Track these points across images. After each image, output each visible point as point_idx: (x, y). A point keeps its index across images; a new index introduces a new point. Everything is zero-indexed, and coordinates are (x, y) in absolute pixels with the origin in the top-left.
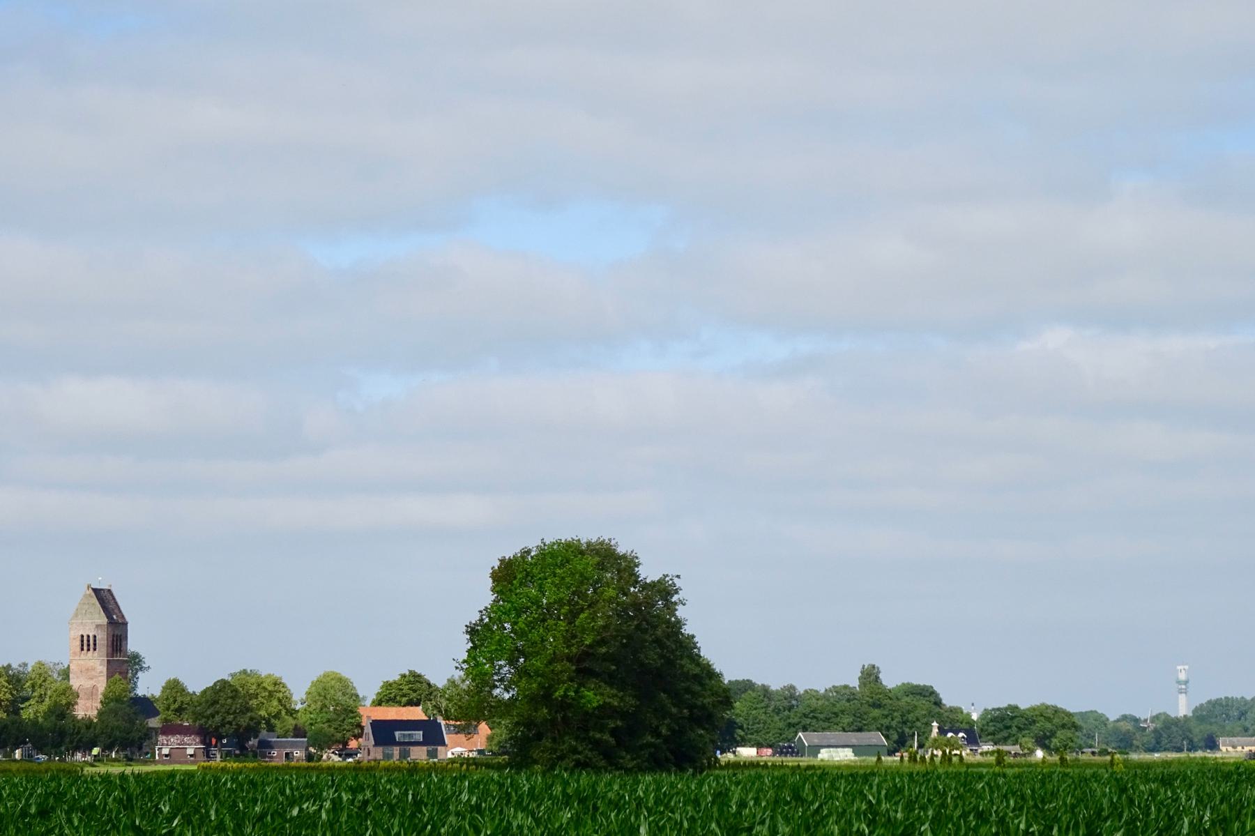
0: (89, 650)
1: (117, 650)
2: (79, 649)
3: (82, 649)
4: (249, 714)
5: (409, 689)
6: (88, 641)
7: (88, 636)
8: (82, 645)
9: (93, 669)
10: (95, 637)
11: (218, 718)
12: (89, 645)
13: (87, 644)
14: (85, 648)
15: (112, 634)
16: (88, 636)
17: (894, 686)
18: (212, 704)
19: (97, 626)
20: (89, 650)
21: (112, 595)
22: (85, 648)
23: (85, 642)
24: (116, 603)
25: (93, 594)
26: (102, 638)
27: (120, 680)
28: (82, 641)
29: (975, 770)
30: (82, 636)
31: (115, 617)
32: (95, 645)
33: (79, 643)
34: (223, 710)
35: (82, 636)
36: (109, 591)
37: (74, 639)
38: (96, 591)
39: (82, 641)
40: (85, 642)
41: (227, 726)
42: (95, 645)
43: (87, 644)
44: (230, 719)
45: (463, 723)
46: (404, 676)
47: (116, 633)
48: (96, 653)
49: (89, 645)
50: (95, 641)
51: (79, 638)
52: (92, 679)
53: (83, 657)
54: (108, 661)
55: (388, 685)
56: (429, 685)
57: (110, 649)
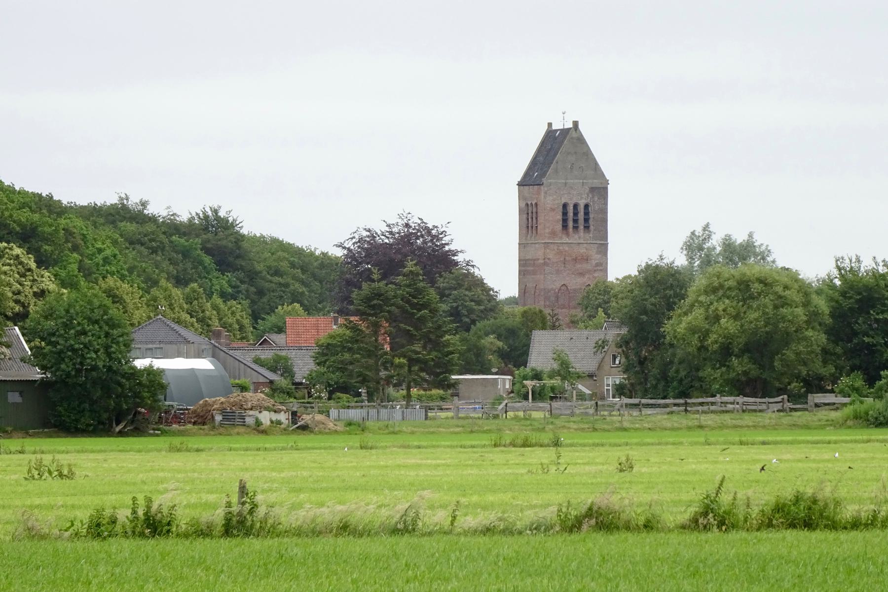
2: (559, 226)
10: (565, 227)
14: (571, 224)
16: (576, 206)
22: (571, 224)
23: (571, 214)
30: (565, 206)
32: (586, 220)
33: (559, 217)
40: (571, 214)
42: (586, 220)
50: (587, 213)
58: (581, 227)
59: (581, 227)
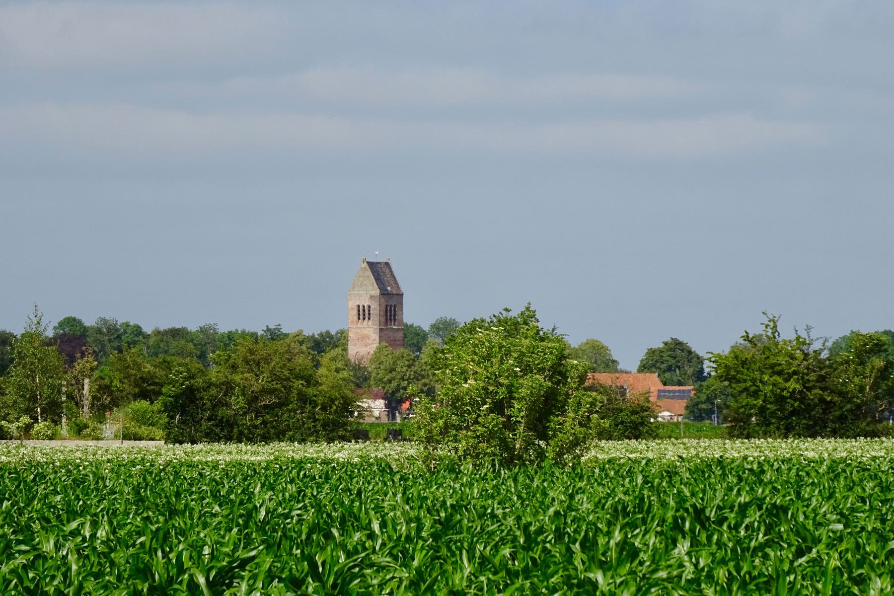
0: (364, 319)
1: (391, 320)
2: (356, 318)
3: (359, 319)
4: (423, 381)
5: (668, 356)
6: (364, 311)
7: (391, 306)
8: (359, 315)
9: (368, 337)
10: (369, 307)
11: (394, 384)
12: (364, 315)
13: (363, 313)
14: (361, 317)
15: (384, 305)
16: (364, 306)
17: (89, 325)
18: (390, 372)
19: (371, 297)
20: (364, 319)
21: (390, 269)
22: (361, 317)
23: (367, 312)
24: (394, 277)
25: (367, 267)
26: (375, 308)
27: (387, 347)
28: (359, 311)
29: (755, 537)
30: (359, 306)
31: (389, 288)
32: (369, 314)
33: (356, 312)
34: (399, 377)
35: (359, 306)
36: (387, 264)
37: (352, 309)
38: (371, 265)
39: (359, 311)
40: (367, 312)
41: (402, 391)
43: (363, 313)
44: (405, 385)
45: (178, 416)
46: (666, 344)
47: (389, 304)
48: (370, 322)
49: (364, 315)
51: (356, 308)
52: (366, 346)
53: (359, 325)
54: (381, 330)
55: (651, 352)
56: (690, 352)
57: (383, 319)
58: (367, 319)
59: (367, 319)
